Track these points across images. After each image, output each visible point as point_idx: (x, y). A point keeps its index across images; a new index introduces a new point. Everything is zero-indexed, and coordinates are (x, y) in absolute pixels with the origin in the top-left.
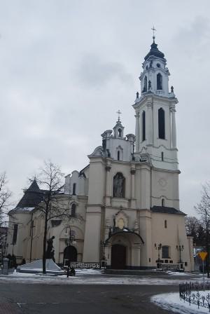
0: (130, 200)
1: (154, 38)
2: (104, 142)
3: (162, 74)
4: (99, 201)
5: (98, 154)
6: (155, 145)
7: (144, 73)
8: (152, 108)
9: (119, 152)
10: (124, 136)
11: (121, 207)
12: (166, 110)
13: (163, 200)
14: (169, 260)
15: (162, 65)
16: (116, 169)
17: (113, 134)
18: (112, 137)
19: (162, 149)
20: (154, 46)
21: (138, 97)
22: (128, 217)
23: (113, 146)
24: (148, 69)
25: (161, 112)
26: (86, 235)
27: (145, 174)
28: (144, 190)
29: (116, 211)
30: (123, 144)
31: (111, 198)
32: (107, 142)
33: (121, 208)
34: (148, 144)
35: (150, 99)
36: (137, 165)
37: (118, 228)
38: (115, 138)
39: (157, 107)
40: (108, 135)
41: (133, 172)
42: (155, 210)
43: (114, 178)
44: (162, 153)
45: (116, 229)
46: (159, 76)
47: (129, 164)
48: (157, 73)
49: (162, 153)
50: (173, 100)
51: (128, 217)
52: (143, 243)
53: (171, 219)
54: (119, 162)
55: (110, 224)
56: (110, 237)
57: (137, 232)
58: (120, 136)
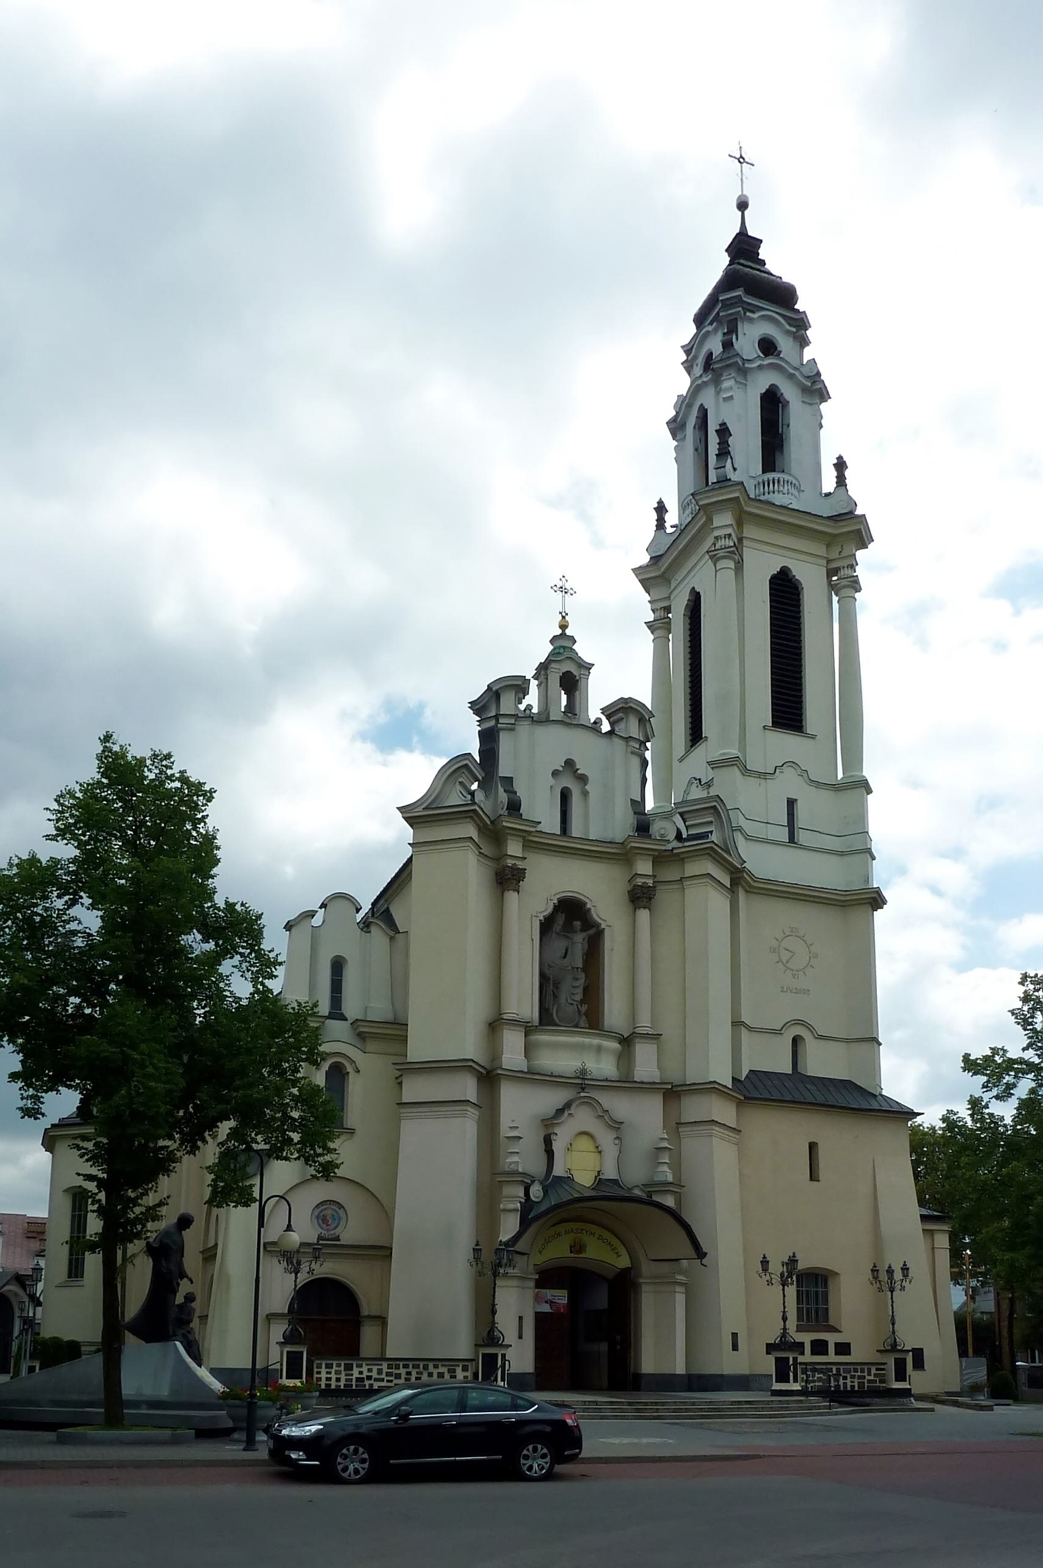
0: (627, 1042)
1: (742, 205)
2: (488, 738)
3: (789, 392)
4: (469, 1045)
5: (455, 798)
6: (754, 763)
7: (695, 390)
8: (739, 567)
9: (565, 796)
10: (594, 712)
11: (583, 1073)
12: (810, 577)
13: (796, 1041)
14: (831, 1339)
15: (785, 344)
16: (549, 880)
17: (532, 699)
18: (527, 716)
19: (789, 785)
20: (744, 248)
21: (661, 524)
22: (617, 1126)
23: (532, 764)
24: (709, 364)
25: (785, 593)
26: (398, 1220)
27: (707, 905)
28: (699, 983)
29: (553, 1098)
30: (589, 754)
31: (529, 1030)
32: (505, 744)
33: (582, 1084)
34: (716, 754)
35: (724, 520)
36: (661, 859)
37: (567, 1180)
38: (542, 719)
39: (762, 565)
40: (507, 704)
41: (640, 897)
42: (755, 1091)
43: (546, 926)
44: (791, 803)
45: (552, 1182)
46: (772, 402)
47: (619, 854)
48: (762, 382)
49: (791, 803)
50: (846, 531)
51: (617, 1126)
52: (700, 1254)
53: (838, 1137)
54: (564, 844)
55: (524, 1158)
56: (525, 1222)
57: (669, 1201)
58: (570, 707)
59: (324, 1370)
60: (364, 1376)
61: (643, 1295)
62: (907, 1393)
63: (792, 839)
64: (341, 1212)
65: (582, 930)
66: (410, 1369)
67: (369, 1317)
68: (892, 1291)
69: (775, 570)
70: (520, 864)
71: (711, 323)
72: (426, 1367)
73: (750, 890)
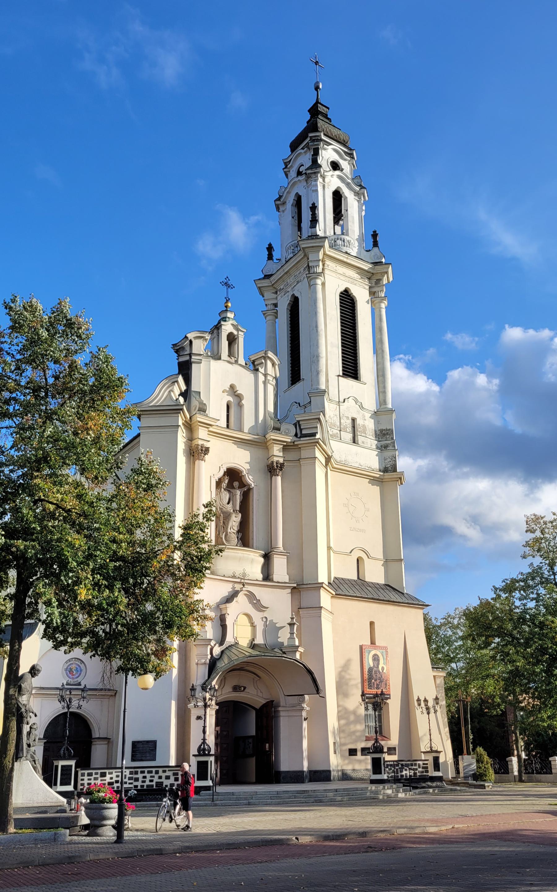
52: (318, 691)
59: (86, 778)
60: (113, 781)
61: (281, 718)
62: (440, 779)
63: (354, 441)
64: (82, 666)
65: (239, 488)
66: (153, 774)
67: (99, 738)
68: (428, 713)
69: (342, 289)
70: (207, 445)
71: (303, 149)
72: (157, 772)
73: (334, 469)
